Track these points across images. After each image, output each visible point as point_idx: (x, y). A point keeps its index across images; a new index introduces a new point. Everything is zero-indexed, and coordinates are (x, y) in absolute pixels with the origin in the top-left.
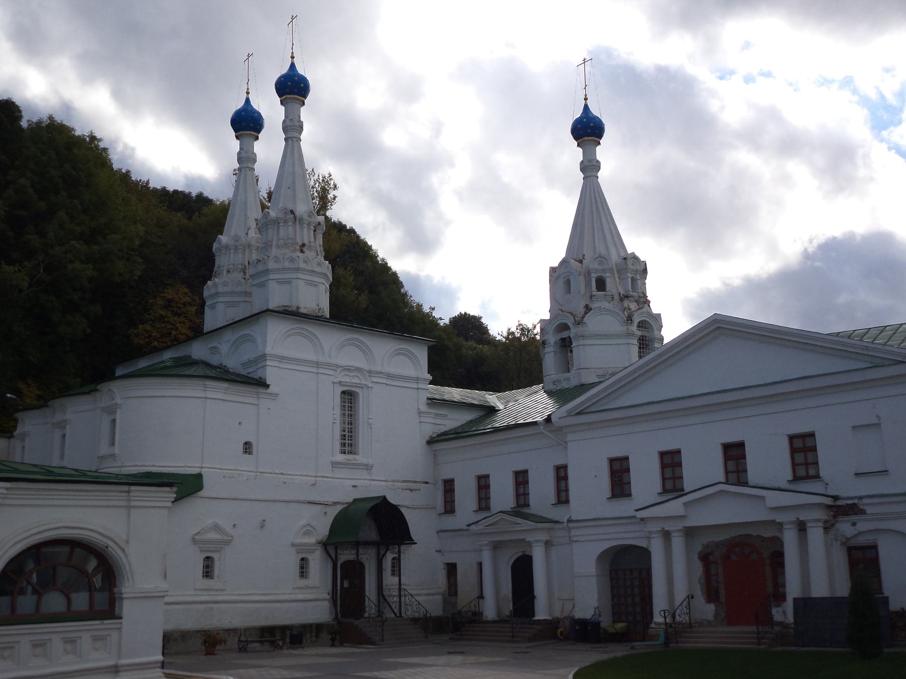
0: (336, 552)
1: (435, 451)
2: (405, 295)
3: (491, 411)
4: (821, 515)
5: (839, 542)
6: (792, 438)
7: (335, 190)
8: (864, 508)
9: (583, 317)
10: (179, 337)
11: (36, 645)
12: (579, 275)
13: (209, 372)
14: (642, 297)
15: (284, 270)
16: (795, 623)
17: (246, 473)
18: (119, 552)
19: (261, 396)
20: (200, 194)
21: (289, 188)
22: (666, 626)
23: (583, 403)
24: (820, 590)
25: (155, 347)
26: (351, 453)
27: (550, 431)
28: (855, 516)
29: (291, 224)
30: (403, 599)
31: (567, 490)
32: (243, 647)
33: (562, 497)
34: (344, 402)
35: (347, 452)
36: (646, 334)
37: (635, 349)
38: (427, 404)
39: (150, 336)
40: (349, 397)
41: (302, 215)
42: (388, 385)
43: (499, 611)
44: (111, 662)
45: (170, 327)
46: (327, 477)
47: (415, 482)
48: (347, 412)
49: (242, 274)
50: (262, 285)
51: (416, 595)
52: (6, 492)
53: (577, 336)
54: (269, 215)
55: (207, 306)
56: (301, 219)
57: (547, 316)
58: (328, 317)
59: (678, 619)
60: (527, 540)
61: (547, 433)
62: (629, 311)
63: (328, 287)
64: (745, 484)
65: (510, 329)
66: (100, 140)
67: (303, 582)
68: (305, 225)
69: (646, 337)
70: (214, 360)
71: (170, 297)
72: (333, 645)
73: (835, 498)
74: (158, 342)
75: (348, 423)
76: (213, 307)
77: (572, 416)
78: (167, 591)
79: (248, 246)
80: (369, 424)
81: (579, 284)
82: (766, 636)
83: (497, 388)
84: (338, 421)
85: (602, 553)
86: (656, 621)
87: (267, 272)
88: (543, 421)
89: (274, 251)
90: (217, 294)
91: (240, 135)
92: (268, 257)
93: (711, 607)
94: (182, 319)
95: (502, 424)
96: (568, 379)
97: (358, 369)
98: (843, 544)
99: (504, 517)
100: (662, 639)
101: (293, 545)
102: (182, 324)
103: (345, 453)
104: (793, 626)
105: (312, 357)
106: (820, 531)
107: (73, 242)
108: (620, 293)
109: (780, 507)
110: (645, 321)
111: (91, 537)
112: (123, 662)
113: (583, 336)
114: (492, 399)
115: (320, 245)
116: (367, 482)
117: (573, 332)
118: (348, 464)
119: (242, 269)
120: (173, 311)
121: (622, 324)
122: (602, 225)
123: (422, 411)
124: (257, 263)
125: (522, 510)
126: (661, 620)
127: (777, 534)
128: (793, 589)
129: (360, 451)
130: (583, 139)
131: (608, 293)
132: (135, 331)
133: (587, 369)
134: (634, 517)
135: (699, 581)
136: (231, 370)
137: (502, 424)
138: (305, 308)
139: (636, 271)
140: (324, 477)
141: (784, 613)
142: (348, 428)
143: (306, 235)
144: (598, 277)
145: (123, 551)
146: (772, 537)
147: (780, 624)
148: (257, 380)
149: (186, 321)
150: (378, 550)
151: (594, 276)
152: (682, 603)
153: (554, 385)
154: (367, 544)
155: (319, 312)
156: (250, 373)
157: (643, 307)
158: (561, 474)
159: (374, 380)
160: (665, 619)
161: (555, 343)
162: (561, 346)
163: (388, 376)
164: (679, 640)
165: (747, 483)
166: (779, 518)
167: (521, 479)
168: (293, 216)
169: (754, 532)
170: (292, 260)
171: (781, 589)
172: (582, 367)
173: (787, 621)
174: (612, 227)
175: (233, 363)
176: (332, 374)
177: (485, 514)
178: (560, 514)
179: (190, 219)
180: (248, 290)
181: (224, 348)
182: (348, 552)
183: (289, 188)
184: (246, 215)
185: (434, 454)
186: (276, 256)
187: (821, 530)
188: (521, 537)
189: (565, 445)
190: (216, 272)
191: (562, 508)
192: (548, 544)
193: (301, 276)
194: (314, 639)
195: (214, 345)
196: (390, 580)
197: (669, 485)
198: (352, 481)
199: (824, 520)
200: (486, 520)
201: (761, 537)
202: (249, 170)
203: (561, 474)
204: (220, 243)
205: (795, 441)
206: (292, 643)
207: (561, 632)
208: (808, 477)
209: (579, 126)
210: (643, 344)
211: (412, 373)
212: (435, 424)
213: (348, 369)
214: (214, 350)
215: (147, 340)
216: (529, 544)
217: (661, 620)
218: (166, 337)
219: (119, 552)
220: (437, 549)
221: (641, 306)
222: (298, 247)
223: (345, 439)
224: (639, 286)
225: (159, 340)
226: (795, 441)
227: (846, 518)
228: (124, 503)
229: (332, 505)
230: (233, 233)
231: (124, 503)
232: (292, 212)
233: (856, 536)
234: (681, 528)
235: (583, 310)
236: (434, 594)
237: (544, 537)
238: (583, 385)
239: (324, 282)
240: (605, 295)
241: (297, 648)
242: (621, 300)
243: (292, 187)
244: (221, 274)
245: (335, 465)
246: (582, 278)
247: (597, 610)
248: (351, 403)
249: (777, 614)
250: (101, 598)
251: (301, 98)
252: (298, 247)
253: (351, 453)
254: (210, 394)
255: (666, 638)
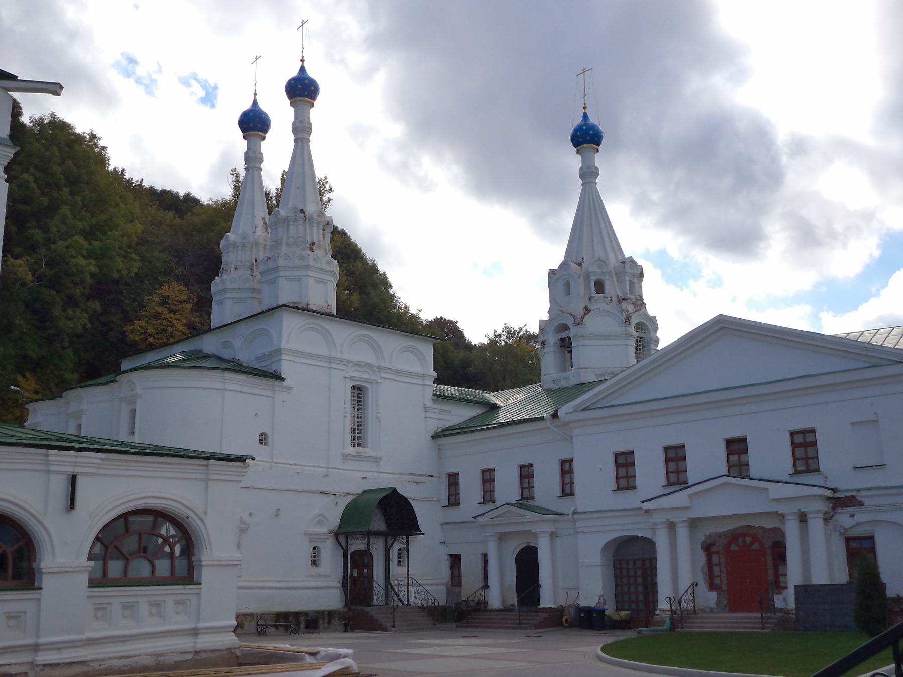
0: (347, 542)
1: (440, 445)
2: (394, 296)
3: (494, 408)
4: (823, 506)
5: (838, 533)
6: (792, 434)
7: (330, 192)
8: (862, 500)
9: (583, 318)
10: (176, 334)
11: (125, 607)
12: (579, 277)
13: (225, 365)
14: (639, 300)
15: (295, 267)
16: (796, 608)
17: (261, 463)
18: (199, 522)
19: (277, 389)
20: (188, 194)
21: (298, 188)
22: (672, 613)
23: (595, 395)
24: (820, 577)
25: (151, 344)
26: (360, 445)
27: (555, 427)
28: (853, 508)
29: (301, 222)
30: (411, 588)
31: (572, 483)
32: (262, 630)
33: (567, 491)
34: (354, 397)
35: (356, 445)
36: (643, 336)
37: (632, 350)
38: (433, 400)
39: (146, 332)
40: (359, 392)
41: (312, 215)
42: (397, 381)
43: (503, 601)
44: (192, 626)
45: (166, 324)
46: (339, 469)
47: (421, 475)
48: (356, 406)
49: (249, 271)
50: (273, 282)
51: (425, 585)
52: (101, 462)
53: (576, 336)
54: (280, 214)
55: (214, 302)
56: (311, 218)
57: (546, 317)
58: (335, 314)
59: (683, 604)
60: (532, 531)
61: (554, 429)
62: (626, 313)
63: (335, 285)
64: (748, 477)
65: (495, 332)
66: (99, 139)
67: (314, 570)
68: (315, 225)
69: (642, 338)
70: (226, 354)
71: (167, 294)
72: (346, 631)
73: (834, 490)
74: (154, 338)
75: (358, 417)
76: (221, 303)
77: (578, 411)
78: (240, 560)
79: (256, 244)
80: (378, 418)
81: (579, 287)
82: (769, 621)
83: (496, 388)
84: (349, 415)
85: (606, 544)
86: (661, 608)
87: (277, 269)
88: (549, 416)
89: (284, 249)
90: (225, 290)
91: (248, 135)
92: (279, 254)
93: (714, 595)
94: (178, 316)
95: (507, 419)
96: (567, 378)
97: (368, 365)
98: (841, 534)
99: (510, 509)
100: (667, 625)
101: (306, 534)
102: (178, 321)
103: (354, 446)
104: (794, 612)
105: (324, 351)
106: (821, 522)
107: (77, 237)
108: (618, 296)
109: (781, 499)
110: (642, 322)
111: (174, 507)
112: (202, 625)
113: (583, 336)
114: (493, 397)
115: (328, 244)
116: (376, 475)
117: (572, 333)
118: (360, 457)
119: (250, 266)
120: (169, 308)
121: (621, 325)
122: (600, 229)
123: (428, 406)
124: (268, 260)
125: (527, 503)
126: (667, 607)
127: (778, 525)
128: (794, 575)
129: (369, 445)
130: (582, 146)
131: (606, 295)
132: (132, 328)
133: (586, 368)
134: (641, 508)
135: (702, 570)
136: (244, 364)
137: (507, 419)
138: (315, 305)
139: (633, 275)
140: (335, 468)
141: (786, 600)
142: (358, 422)
143: (315, 234)
144: (597, 279)
145: (202, 520)
146: (773, 528)
147: (781, 610)
148: (272, 373)
149: (182, 318)
150: (386, 541)
151: (593, 278)
152: (687, 590)
153: (554, 383)
154: (377, 534)
155: (327, 309)
156: (264, 366)
157: (640, 310)
158: (567, 468)
159: (384, 375)
160: (671, 607)
161: (555, 343)
162: (561, 346)
163: (396, 372)
164: (685, 625)
165: (750, 476)
166: (781, 509)
167: (526, 473)
168: (303, 215)
169: (756, 523)
170: (302, 258)
171: (781, 579)
172: (581, 366)
173: (788, 608)
174: (610, 232)
175: (245, 356)
176: (343, 369)
177: (491, 506)
178: (565, 505)
179: (181, 217)
180: (256, 286)
181: (237, 343)
182: (359, 541)
183: (298, 188)
184: (253, 213)
185: (439, 449)
186: (286, 254)
187: (821, 521)
188: (527, 528)
189: (571, 440)
190: (223, 269)
191: (568, 500)
192: (553, 535)
193: (310, 273)
194: (326, 625)
195: (226, 339)
196: (398, 571)
197: (673, 478)
198: (362, 473)
199: (824, 512)
200: (492, 512)
201: (763, 527)
202: (257, 170)
203: (567, 468)
204: (228, 240)
205: (795, 436)
206: (307, 627)
207: (567, 620)
208: (808, 471)
209: (579, 134)
210: (640, 345)
211: (417, 368)
212: (439, 419)
213: (358, 364)
214: (226, 344)
215: (143, 337)
216: (535, 535)
217: (667, 607)
218: (161, 334)
219: (199, 522)
220: (442, 541)
221: (638, 308)
222: (308, 246)
223: (354, 433)
224: (636, 290)
225: (155, 336)
226: (795, 436)
227: (845, 510)
228: (201, 476)
229: (342, 496)
230: (240, 231)
231: (201, 476)
232: (302, 211)
233: (854, 526)
234: (686, 519)
235: (582, 312)
236: (438, 585)
237: (549, 527)
238: (582, 384)
239: (332, 280)
240: (604, 297)
241: (312, 633)
242: (619, 302)
243: (302, 188)
244: (229, 271)
245: (346, 457)
246: (581, 281)
247: (602, 598)
248: (360, 398)
249: (778, 603)
250: (181, 565)
251: (311, 100)
252: (308, 246)
253: (360, 446)
254: (228, 386)
255: (672, 624)
